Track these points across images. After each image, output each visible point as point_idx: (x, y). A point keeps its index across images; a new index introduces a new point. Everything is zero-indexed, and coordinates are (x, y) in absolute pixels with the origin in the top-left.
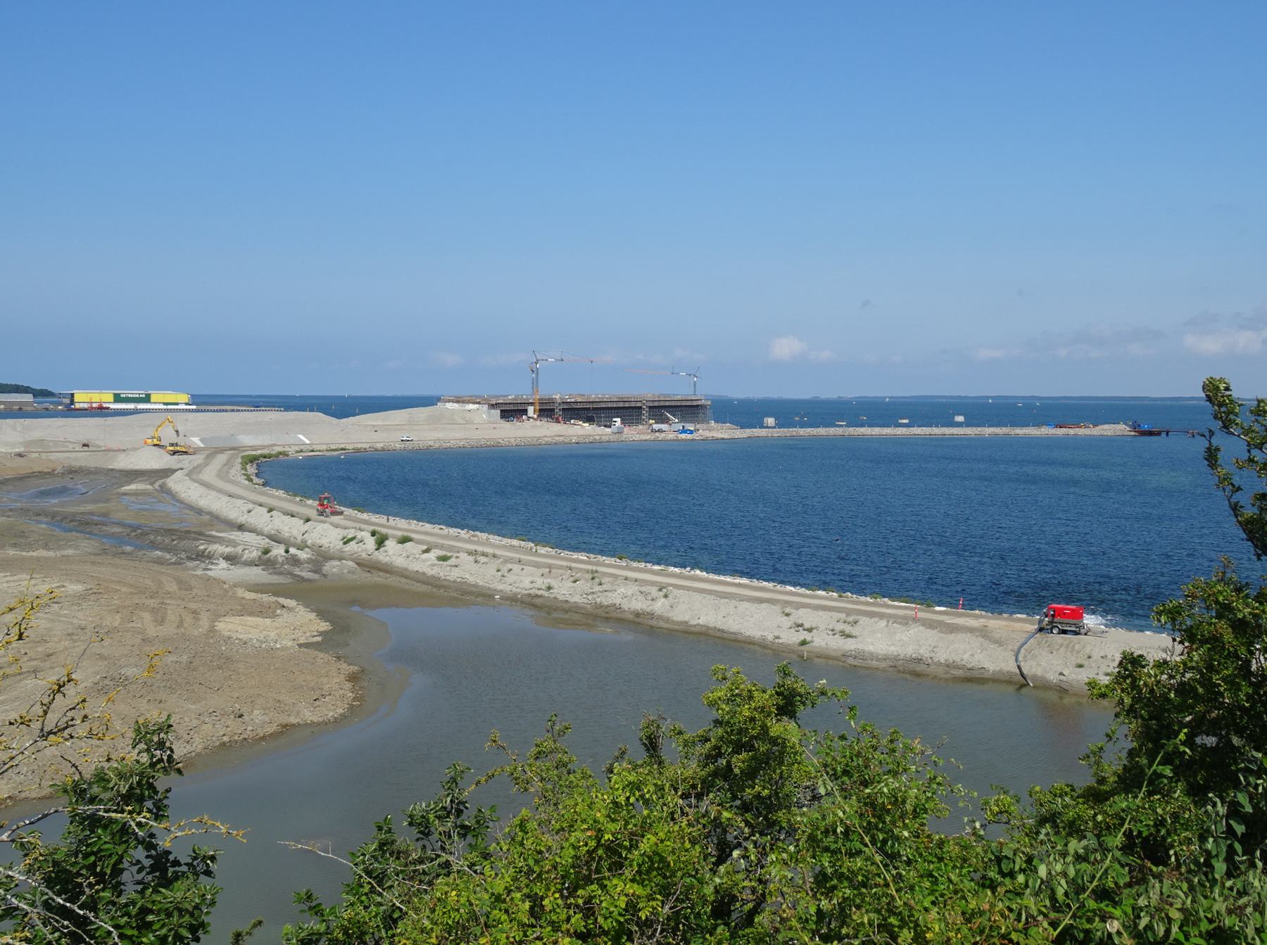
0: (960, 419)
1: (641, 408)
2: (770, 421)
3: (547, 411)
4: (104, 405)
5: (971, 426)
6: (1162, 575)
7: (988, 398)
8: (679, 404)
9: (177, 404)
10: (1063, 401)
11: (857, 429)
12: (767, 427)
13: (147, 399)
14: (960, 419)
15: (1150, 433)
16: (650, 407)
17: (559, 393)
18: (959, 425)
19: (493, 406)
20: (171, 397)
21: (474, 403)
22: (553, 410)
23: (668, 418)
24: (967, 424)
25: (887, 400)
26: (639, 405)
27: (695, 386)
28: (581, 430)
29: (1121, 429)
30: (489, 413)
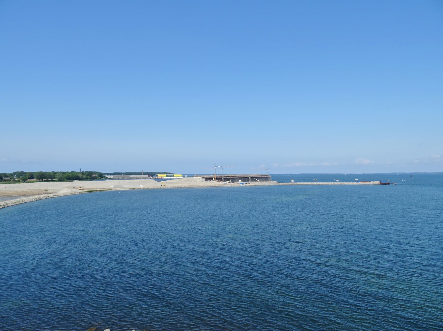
0: (357, 179)
1: (249, 178)
2: (292, 181)
3: (218, 179)
4: (162, 177)
5: (340, 182)
6: (55, 204)
7: (388, 173)
8: (233, 177)
9: (179, 177)
10: (434, 174)
11: (297, 183)
12: (292, 182)
13: (173, 176)
14: (357, 179)
15: (385, 184)
16: (251, 177)
17: (219, 172)
18: (356, 181)
19: (203, 178)
20: (178, 175)
21: (199, 177)
22: (221, 178)
23: (256, 180)
24: (339, 181)
25: (389, 174)
26: (248, 177)
27: (222, 172)
28: (228, 184)
29: (377, 183)
30: (202, 179)
